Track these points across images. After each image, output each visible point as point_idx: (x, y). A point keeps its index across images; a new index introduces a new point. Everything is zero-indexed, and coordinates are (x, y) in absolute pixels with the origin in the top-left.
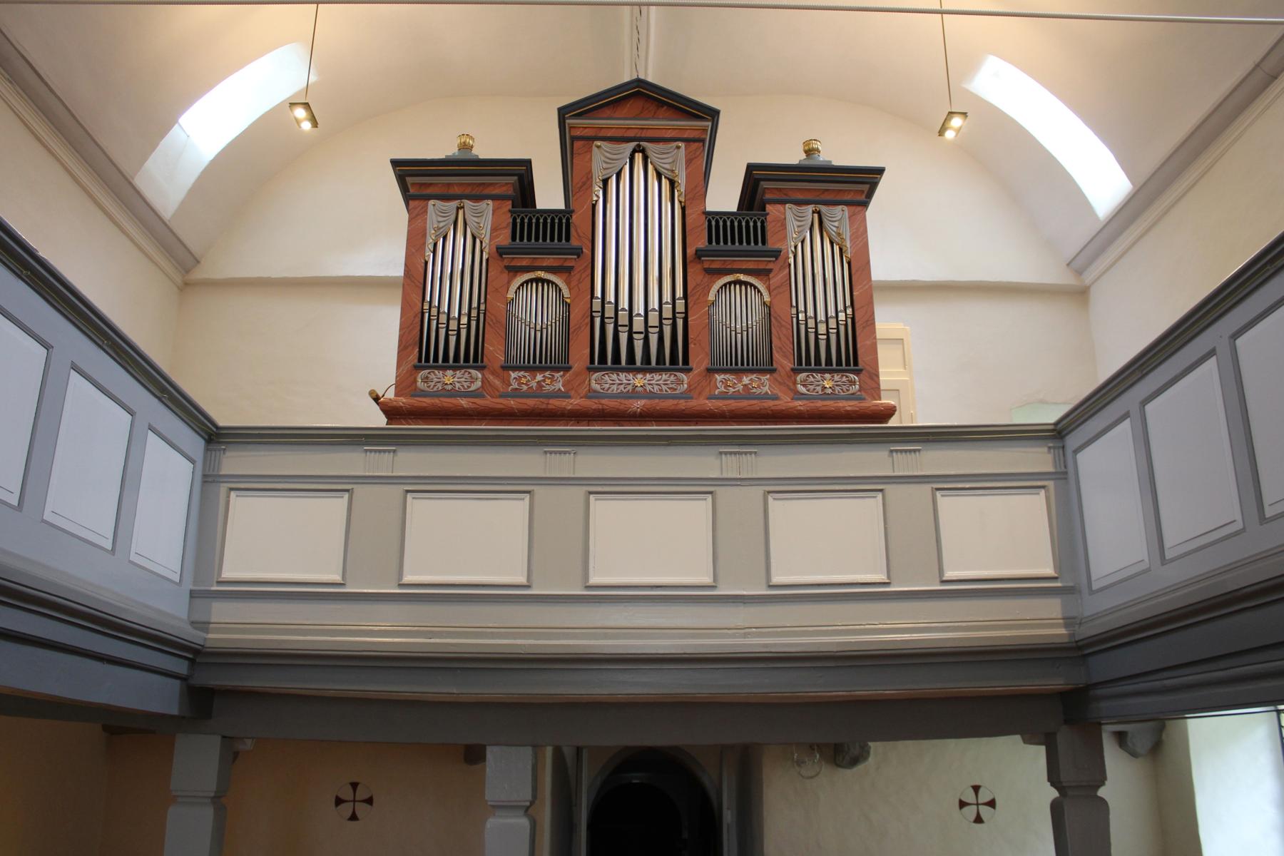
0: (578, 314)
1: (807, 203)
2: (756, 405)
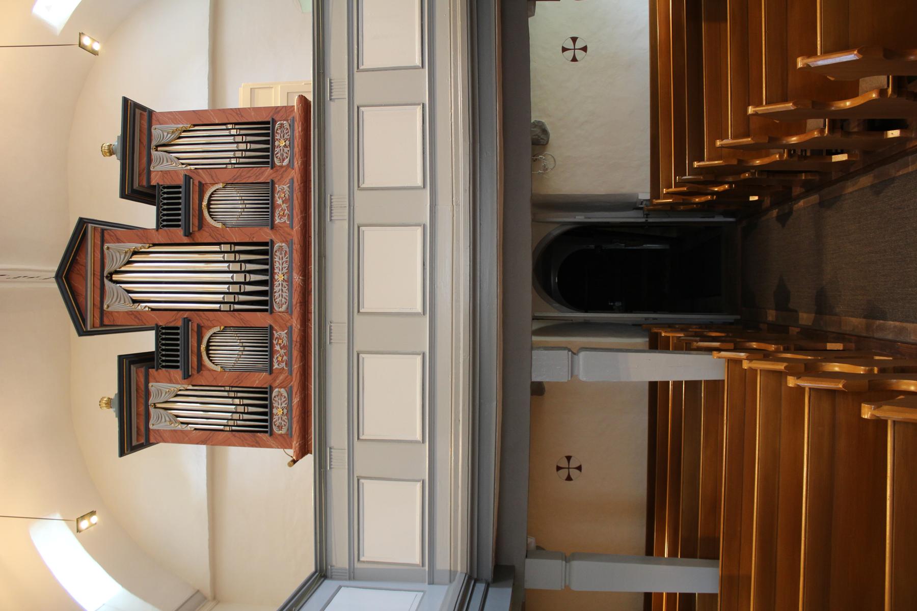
0: (231, 321)
1: (150, 155)
2: (297, 195)
